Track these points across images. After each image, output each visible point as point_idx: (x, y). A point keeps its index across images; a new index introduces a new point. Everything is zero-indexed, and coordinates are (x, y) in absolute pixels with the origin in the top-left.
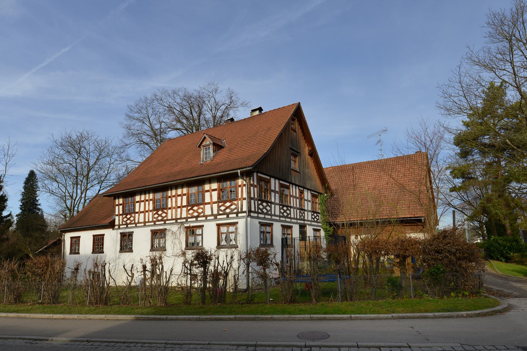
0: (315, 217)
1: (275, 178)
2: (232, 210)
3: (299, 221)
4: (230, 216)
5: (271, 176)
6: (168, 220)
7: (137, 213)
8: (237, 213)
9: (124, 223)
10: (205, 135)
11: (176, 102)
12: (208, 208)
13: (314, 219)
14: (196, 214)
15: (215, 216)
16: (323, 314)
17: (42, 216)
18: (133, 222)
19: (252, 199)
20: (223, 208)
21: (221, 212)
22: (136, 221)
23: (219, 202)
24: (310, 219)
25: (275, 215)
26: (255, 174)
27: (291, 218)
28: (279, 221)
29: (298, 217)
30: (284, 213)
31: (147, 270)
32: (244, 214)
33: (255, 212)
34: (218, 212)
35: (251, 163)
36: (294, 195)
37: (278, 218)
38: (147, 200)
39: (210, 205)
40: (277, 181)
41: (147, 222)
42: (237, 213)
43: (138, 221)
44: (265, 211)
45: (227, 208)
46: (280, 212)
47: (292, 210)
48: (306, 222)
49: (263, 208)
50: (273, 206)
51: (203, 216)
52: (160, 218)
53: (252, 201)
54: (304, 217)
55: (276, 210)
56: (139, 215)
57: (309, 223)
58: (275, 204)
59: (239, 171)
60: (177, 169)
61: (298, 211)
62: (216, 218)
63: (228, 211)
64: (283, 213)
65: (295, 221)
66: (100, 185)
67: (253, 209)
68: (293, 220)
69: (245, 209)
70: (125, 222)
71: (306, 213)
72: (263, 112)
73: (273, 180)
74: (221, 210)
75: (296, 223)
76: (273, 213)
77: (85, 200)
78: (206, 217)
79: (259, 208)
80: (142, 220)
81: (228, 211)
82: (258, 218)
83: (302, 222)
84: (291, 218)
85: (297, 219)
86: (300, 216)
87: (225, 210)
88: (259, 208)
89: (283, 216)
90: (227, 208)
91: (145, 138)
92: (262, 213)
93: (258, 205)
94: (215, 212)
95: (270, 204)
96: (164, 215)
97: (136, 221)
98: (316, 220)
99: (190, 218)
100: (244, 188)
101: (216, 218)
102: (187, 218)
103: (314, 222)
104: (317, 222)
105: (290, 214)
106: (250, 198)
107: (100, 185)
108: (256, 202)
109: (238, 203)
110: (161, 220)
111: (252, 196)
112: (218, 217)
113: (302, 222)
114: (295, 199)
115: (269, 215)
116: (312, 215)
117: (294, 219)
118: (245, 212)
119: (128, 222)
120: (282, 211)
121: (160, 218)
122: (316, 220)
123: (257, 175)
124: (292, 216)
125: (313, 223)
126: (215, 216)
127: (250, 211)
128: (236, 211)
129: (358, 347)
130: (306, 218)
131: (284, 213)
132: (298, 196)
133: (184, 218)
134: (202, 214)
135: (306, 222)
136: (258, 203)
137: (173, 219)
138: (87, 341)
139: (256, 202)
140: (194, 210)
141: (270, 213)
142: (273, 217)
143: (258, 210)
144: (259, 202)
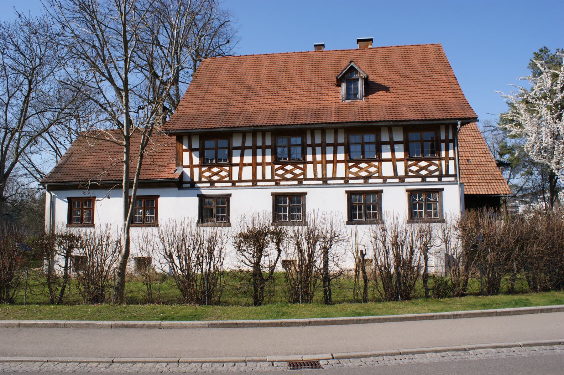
2: (431, 172)
6: (306, 179)
8: (440, 177)
14: (364, 174)
15: (402, 180)
16: (392, 315)
18: (227, 179)
20: (207, 174)
21: (410, 174)
23: (408, 160)
31: (257, 265)
34: (406, 172)
41: (330, 179)
42: (440, 177)
45: (422, 169)
51: (378, 178)
52: (289, 176)
56: (241, 170)
63: (424, 172)
70: (206, 178)
78: (385, 179)
81: (424, 172)
87: (418, 171)
90: (422, 169)
96: (298, 171)
99: (352, 178)
101: (346, 182)
109: (441, 165)
112: (407, 180)
119: (215, 178)
126: (402, 180)
128: (437, 173)
129: (245, 361)
137: (319, 179)
140: (361, 169)
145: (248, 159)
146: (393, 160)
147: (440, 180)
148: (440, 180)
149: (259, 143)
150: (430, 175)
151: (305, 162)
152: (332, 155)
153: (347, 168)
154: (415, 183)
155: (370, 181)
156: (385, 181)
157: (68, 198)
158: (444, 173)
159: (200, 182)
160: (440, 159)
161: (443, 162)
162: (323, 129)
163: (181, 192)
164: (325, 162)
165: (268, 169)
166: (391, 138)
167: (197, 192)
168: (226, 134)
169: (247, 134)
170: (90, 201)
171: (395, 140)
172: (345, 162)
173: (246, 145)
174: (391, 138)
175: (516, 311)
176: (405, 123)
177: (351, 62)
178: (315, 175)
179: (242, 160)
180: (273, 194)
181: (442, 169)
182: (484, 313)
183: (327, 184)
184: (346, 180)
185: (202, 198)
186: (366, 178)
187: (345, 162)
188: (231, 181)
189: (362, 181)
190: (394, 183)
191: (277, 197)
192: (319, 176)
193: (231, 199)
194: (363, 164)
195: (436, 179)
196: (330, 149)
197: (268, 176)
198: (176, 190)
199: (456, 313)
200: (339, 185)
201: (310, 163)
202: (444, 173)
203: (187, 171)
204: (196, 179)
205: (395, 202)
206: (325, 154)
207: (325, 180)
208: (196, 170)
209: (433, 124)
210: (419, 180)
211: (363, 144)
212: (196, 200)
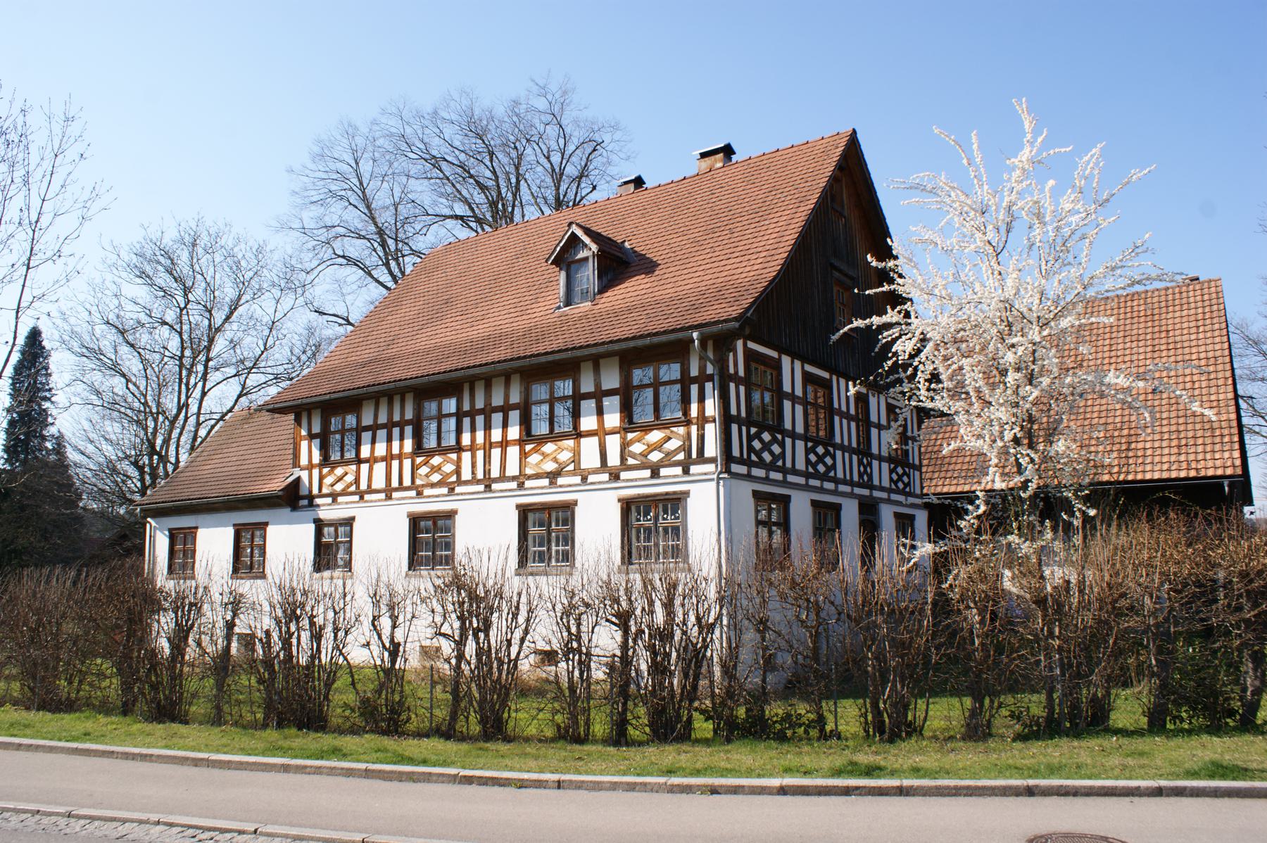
0: (900, 478)
1: (794, 356)
2: (669, 454)
3: (857, 491)
4: (663, 472)
5: (781, 351)
7: (367, 461)
9: (325, 491)
10: (575, 229)
11: (449, 139)
12: (589, 446)
13: (896, 483)
14: (550, 466)
17: (62, 465)
18: (353, 488)
19: (737, 418)
20: (637, 448)
21: (631, 461)
22: (363, 486)
23: (626, 430)
24: (886, 483)
25: (795, 472)
26: (740, 343)
27: (835, 480)
28: (807, 488)
29: (856, 478)
30: (817, 463)
32: (710, 468)
33: (741, 461)
34: (623, 459)
35: (735, 311)
36: (844, 408)
37: (802, 480)
38: (395, 424)
39: (596, 439)
40: (798, 364)
43: (369, 486)
44: (767, 457)
45: (653, 447)
46: (808, 461)
47: (839, 454)
48: (876, 494)
49: (762, 450)
50: (788, 441)
51: (573, 473)
53: (735, 427)
54: (870, 477)
55: (798, 454)
57: (884, 495)
58: (793, 435)
59: (695, 335)
60: (481, 330)
61: (855, 458)
62: (615, 477)
64: (814, 466)
65: (847, 489)
66: (242, 378)
67: (736, 452)
68: (842, 488)
69: (712, 449)
71: (875, 463)
72: (734, 158)
73: (786, 361)
74: (633, 456)
75: (851, 495)
76: (789, 465)
77: (198, 424)
79: (751, 449)
80: (379, 482)
81: (655, 457)
82: (749, 477)
83: (866, 492)
84: (835, 480)
85: (851, 483)
86: (861, 475)
87: (644, 455)
88: (751, 449)
89: (816, 475)
91: (356, 248)
92: (761, 464)
93: (750, 438)
94: (614, 460)
95: (779, 437)
97: (363, 486)
98: (901, 485)
100: (709, 386)
102: (890, 491)
103: (898, 492)
104: (903, 492)
105: (834, 467)
106: (727, 420)
107: (242, 378)
108: (744, 429)
110: (440, 484)
111: (734, 411)
112: (624, 475)
113: (866, 492)
114: (845, 421)
115: (778, 470)
116: (891, 471)
117: (844, 482)
118: (712, 460)
120: (813, 458)
121: (436, 478)
122: (901, 485)
123: (745, 345)
124: (840, 475)
125: (894, 497)
127: (728, 457)
128: (681, 456)
130: (876, 482)
131: (817, 463)
132: (852, 411)
133: (514, 478)
134: (571, 467)
135: (876, 494)
136: (748, 431)
137: (479, 482)
138: (166, 824)
139: (744, 429)
140: (545, 455)
141: (780, 463)
142: (791, 478)
143: (749, 456)
144: (753, 430)
145: (381, 449)
146: (601, 433)
147: (686, 471)
148: (686, 471)
149: (397, 418)
150: (667, 461)
151: (459, 448)
152: (595, 418)
153: (524, 455)
154: (638, 483)
155: (560, 481)
156: (584, 479)
157: (170, 530)
158: (694, 455)
159: (322, 496)
160: (688, 422)
161: (694, 428)
162: (484, 377)
163: (296, 514)
164: (488, 446)
165: (513, 451)
166: (598, 384)
167: (310, 514)
168: (349, 403)
169: (494, 380)
170: (191, 533)
171: (605, 387)
172: (521, 442)
173: (583, 391)
174: (598, 384)
175: (241, 763)
176: (624, 345)
177: (570, 225)
178: (473, 473)
179: (342, 456)
180: (518, 506)
181: (690, 446)
182: (187, 759)
183: (491, 491)
184: (520, 480)
185: (320, 525)
186: (553, 476)
187: (521, 442)
188: (577, 470)
189: (546, 482)
190: (600, 483)
191: (524, 512)
192: (480, 475)
193: (578, 510)
194: (655, 432)
195: (678, 470)
196: (588, 405)
197: (512, 470)
198: (286, 511)
199: (145, 751)
200: (505, 494)
201: (590, 434)
202: (694, 455)
203: (304, 475)
204: (315, 491)
205: (598, 527)
206: (490, 428)
207: (488, 482)
208: (316, 472)
209: (553, 362)
210: (647, 473)
211: (552, 402)
212: (311, 528)
